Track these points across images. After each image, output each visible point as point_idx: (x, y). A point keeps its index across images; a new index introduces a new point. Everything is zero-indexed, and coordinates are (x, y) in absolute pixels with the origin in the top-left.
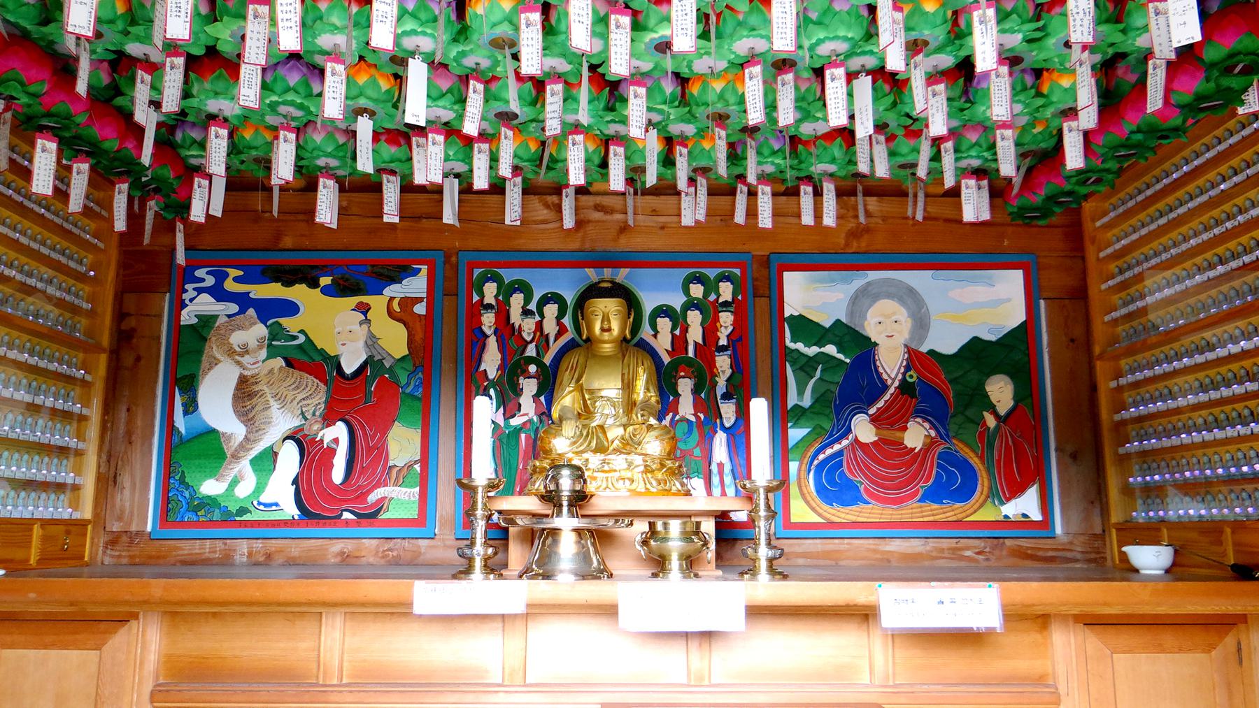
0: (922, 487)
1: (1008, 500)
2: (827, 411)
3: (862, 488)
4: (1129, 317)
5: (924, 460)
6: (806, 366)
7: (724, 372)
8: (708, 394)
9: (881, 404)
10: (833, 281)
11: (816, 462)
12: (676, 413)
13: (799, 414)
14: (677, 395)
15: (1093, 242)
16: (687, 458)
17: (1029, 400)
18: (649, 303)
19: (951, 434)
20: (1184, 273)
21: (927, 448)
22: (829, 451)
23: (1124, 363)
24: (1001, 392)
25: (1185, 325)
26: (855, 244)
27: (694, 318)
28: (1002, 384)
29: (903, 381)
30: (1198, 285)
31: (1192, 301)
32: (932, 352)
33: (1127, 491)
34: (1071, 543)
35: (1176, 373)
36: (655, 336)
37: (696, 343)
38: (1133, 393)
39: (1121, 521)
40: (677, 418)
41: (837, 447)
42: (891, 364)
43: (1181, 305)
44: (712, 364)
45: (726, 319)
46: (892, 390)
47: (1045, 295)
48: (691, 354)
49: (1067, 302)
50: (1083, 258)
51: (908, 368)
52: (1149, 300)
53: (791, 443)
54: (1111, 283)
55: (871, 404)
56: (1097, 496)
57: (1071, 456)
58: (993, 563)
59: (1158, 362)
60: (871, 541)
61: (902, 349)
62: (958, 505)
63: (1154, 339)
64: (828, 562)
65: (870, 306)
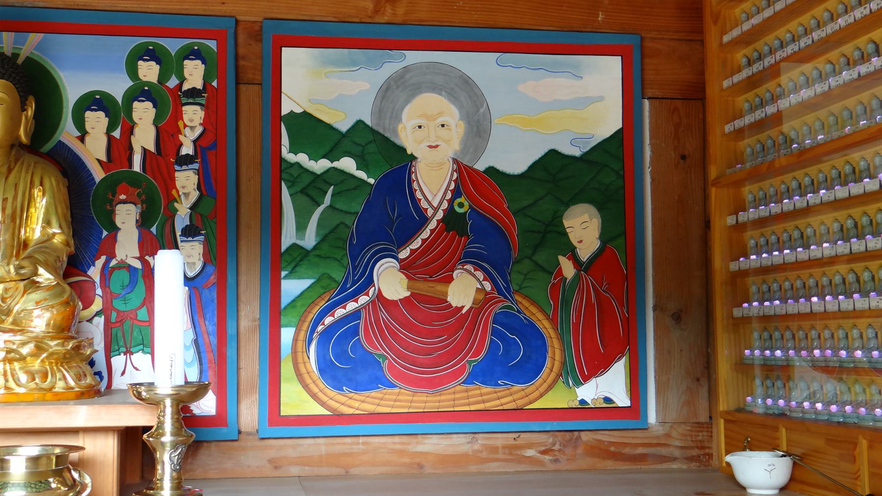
0: (471, 362)
1: (586, 379)
2: (339, 254)
3: (385, 365)
4: (759, 126)
5: (471, 330)
6: (310, 188)
7: (187, 195)
8: (161, 229)
9: (416, 244)
10: (354, 63)
11: (320, 328)
12: (112, 255)
13: (298, 258)
14: (114, 229)
15: (715, 22)
16: (127, 325)
17: (621, 241)
18: (73, 87)
19: (514, 287)
20: (828, 67)
21: (482, 303)
22: (340, 312)
23: (748, 191)
24: (584, 228)
25: (826, 143)
26: (389, 10)
27: (144, 113)
28: (586, 217)
29: (450, 212)
30: (845, 84)
31: (836, 108)
32: (492, 171)
33: (743, 367)
34: (668, 435)
35: (807, 211)
36: (82, 139)
37: (145, 151)
38: (757, 233)
39: (732, 408)
40: (113, 263)
41: (351, 306)
42: (433, 185)
43: (822, 113)
44: (169, 183)
45: (193, 115)
46: (433, 224)
47: (650, 92)
48: (137, 167)
49: (679, 103)
50: (702, 42)
51: (456, 193)
52: (783, 104)
53: (285, 301)
54: (736, 78)
55: (403, 242)
56: (700, 371)
57: (673, 316)
58: (563, 465)
59: (789, 193)
60: (397, 439)
61: (449, 166)
62: (518, 387)
63: (784, 161)
64: (335, 471)
65: (407, 102)
